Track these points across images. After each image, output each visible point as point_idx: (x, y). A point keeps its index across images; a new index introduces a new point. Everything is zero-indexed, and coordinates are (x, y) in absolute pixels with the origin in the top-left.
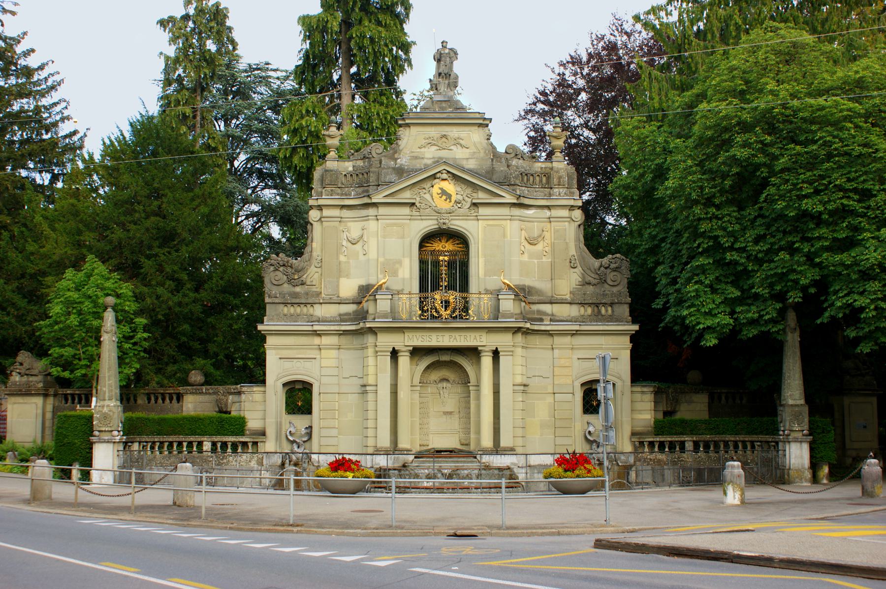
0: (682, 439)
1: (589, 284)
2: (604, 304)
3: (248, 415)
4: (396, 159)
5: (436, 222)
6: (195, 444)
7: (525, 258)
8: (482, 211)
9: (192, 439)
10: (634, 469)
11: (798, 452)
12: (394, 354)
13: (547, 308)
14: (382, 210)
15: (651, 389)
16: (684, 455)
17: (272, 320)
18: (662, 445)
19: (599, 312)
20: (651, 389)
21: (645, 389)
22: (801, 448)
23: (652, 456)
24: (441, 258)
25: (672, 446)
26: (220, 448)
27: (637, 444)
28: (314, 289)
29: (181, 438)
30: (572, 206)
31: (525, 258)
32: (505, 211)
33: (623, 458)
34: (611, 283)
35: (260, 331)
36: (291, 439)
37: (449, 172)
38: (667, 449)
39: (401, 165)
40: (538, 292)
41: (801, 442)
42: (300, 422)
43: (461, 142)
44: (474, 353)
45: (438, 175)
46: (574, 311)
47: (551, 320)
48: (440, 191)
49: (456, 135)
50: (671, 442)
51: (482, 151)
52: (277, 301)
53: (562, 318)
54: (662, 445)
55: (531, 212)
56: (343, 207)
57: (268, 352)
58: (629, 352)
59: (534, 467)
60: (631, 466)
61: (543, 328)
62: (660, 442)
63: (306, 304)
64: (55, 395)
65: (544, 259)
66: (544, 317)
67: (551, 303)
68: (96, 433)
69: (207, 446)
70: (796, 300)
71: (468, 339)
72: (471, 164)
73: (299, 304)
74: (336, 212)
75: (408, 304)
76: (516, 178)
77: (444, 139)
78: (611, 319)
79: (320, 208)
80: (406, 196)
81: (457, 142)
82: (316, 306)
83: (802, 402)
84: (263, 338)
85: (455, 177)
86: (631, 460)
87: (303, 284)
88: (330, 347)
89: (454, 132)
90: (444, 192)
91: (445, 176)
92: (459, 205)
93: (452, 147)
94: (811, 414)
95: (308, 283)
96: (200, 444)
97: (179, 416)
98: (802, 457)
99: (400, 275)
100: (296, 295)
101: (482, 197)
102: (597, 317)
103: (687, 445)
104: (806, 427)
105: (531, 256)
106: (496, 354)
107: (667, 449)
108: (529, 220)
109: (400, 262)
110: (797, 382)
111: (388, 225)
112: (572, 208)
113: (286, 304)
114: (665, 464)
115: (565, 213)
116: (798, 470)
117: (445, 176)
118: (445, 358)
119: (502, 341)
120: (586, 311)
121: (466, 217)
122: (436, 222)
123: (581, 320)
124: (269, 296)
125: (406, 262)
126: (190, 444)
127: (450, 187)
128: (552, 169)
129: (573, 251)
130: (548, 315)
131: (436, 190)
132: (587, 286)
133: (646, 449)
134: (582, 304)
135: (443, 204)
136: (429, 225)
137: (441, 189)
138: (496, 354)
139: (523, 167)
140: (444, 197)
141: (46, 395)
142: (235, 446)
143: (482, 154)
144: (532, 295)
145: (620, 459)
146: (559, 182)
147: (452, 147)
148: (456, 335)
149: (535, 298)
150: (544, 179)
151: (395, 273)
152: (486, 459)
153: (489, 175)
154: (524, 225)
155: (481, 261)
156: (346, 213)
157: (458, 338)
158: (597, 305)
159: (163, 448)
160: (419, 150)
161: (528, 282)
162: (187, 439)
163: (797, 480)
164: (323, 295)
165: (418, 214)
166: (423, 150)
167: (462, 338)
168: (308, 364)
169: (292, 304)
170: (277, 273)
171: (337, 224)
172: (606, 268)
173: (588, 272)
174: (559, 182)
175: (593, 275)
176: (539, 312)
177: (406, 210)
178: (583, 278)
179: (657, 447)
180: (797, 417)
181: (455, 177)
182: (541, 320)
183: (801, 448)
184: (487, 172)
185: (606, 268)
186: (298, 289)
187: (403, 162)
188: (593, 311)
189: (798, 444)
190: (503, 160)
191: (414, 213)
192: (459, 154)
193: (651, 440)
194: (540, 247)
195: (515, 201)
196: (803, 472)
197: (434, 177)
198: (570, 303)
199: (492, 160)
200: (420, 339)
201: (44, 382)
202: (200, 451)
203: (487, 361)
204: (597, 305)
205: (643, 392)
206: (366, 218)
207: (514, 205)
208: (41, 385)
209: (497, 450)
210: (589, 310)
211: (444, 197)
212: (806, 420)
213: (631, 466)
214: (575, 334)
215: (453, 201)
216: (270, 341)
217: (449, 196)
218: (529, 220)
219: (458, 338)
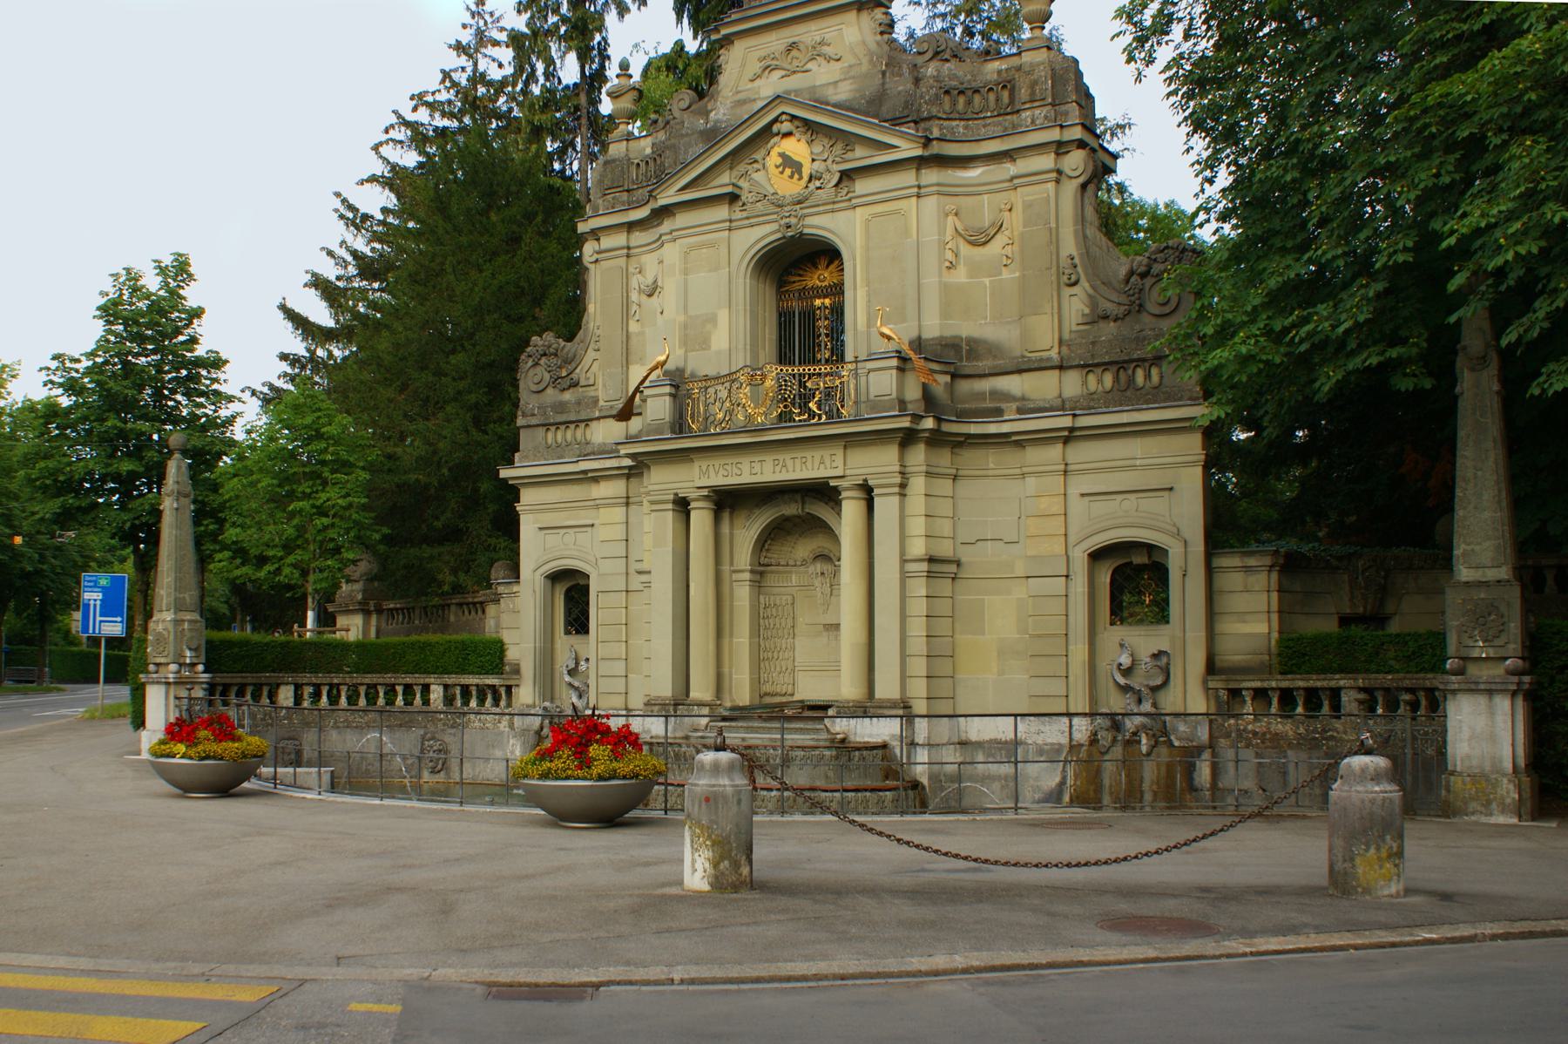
0: (1333, 684)
1: (1106, 317)
2: (1140, 361)
3: (506, 637)
4: (707, 113)
5: (774, 226)
6: (418, 690)
7: (960, 276)
8: (862, 186)
9: (408, 680)
10: (1206, 755)
11: (1481, 723)
12: (682, 506)
13: (1012, 384)
14: (682, 219)
15: (1268, 561)
16: (1338, 724)
17: (526, 457)
18: (1287, 698)
19: (1131, 380)
20: (1268, 561)
21: (1252, 562)
22: (1492, 713)
23: (1259, 727)
24: (818, 302)
25: (1312, 698)
26: (460, 697)
27: (1223, 695)
28: (591, 392)
29: (389, 678)
30: (1060, 144)
31: (960, 276)
32: (907, 178)
33: (1182, 728)
34: (1157, 311)
35: (505, 480)
36: (1122, 681)
37: (793, 118)
38: (1300, 710)
39: (717, 121)
40: (993, 349)
41: (1490, 693)
42: (1143, 641)
43: (826, 49)
44: (825, 492)
45: (775, 128)
46: (1072, 384)
47: (1020, 411)
48: (780, 161)
49: (818, 39)
50: (369, 686)
51: (865, 61)
52: (534, 421)
53: (1042, 404)
54: (1287, 698)
55: (974, 173)
56: (631, 226)
57: (523, 519)
58: (1199, 471)
59: (979, 745)
60: (1199, 750)
61: (1005, 428)
62: (1306, 690)
63: (577, 422)
64: (379, 611)
65: (1006, 274)
66: (1003, 406)
67: (1020, 371)
68: (152, 668)
69: (437, 693)
70: (1400, 258)
71: (809, 464)
72: (843, 93)
73: (567, 423)
74: (619, 239)
75: (753, 407)
76: (930, 102)
77: (794, 53)
78: (1160, 395)
79: (595, 234)
80: (723, 182)
81: (817, 52)
82: (594, 424)
83: (1504, 573)
84: (511, 493)
85: (810, 127)
86: (1203, 734)
87: (575, 385)
88: (609, 503)
89: (808, 33)
90: (788, 162)
91: (786, 126)
92: (818, 184)
93: (809, 66)
94: (1528, 608)
95: (583, 383)
96: (426, 689)
97: (477, 638)
98: (1493, 738)
99: (714, 347)
100: (561, 407)
101: (861, 156)
102: (1125, 394)
103: (1344, 698)
104: (1514, 647)
105: (975, 270)
106: (867, 492)
107: (1300, 710)
108: (972, 191)
109: (713, 319)
110: (1487, 515)
111: (692, 248)
112: (1060, 148)
113: (547, 426)
114: (1290, 745)
115: (1046, 161)
116: (1478, 777)
117: (786, 126)
118: (791, 509)
119: (879, 463)
120: (1100, 381)
121: (832, 207)
122: (774, 226)
123: (1090, 403)
124: (524, 415)
125: (723, 316)
126: (408, 689)
127: (796, 147)
128: (1019, 69)
129: (1069, 246)
130: (1013, 398)
131: (774, 160)
132: (1102, 324)
133: (1249, 708)
134: (1088, 367)
135: (788, 187)
136: (759, 235)
137: (782, 155)
138: (867, 492)
139: (955, 77)
140: (788, 171)
141: (367, 613)
142: (482, 693)
143: (865, 67)
144: (977, 358)
145: (1175, 730)
146: (1033, 93)
147: (809, 66)
148: (786, 456)
149: (984, 364)
150: (1006, 94)
151: (705, 344)
152: (840, 726)
153: (873, 106)
154: (951, 204)
155: (861, 293)
156: (639, 238)
157: (790, 463)
158: (1119, 365)
159: (260, 696)
160: (750, 85)
161: (966, 329)
162: (367, 681)
163: (1473, 805)
164: (601, 403)
165: (745, 214)
166: (757, 83)
167: (798, 461)
168: (583, 537)
169: (557, 425)
170: (538, 370)
171: (622, 261)
172: (1143, 276)
173: (1103, 289)
174: (1033, 93)
175: (1114, 297)
176: (995, 394)
177: (722, 212)
178: (1093, 302)
179: (1275, 701)
180: (1484, 618)
181: (810, 127)
182: (998, 412)
183: (1492, 713)
184: (871, 102)
185: (1143, 276)
186: (567, 396)
187: (720, 116)
188: (1116, 379)
189: (1482, 700)
190: (905, 70)
191: (738, 215)
192: (822, 75)
193: (1257, 684)
194: (995, 247)
195: (919, 152)
196: (1496, 784)
197: (766, 133)
198: (1061, 368)
199: (884, 73)
200: (722, 472)
201: (365, 591)
202: (426, 702)
203: (851, 509)
204: (1119, 365)
205: (1247, 569)
206: (659, 242)
207: (920, 162)
208: (360, 597)
209: (866, 708)
210: (1108, 380)
211: (788, 171)
212: (1514, 627)
213: (1199, 750)
214: (1070, 437)
215: (806, 178)
216: (528, 497)
217: (796, 167)
218: (972, 191)
219: (790, 463)
